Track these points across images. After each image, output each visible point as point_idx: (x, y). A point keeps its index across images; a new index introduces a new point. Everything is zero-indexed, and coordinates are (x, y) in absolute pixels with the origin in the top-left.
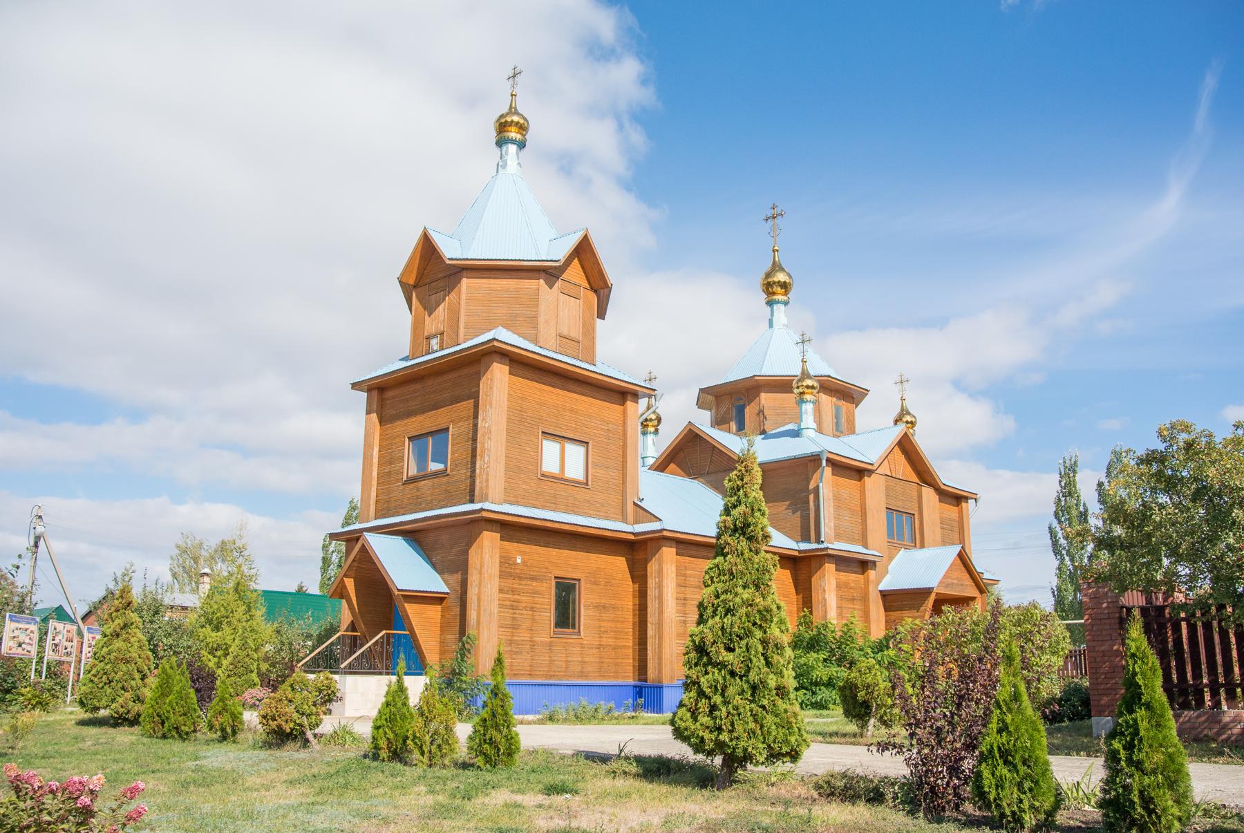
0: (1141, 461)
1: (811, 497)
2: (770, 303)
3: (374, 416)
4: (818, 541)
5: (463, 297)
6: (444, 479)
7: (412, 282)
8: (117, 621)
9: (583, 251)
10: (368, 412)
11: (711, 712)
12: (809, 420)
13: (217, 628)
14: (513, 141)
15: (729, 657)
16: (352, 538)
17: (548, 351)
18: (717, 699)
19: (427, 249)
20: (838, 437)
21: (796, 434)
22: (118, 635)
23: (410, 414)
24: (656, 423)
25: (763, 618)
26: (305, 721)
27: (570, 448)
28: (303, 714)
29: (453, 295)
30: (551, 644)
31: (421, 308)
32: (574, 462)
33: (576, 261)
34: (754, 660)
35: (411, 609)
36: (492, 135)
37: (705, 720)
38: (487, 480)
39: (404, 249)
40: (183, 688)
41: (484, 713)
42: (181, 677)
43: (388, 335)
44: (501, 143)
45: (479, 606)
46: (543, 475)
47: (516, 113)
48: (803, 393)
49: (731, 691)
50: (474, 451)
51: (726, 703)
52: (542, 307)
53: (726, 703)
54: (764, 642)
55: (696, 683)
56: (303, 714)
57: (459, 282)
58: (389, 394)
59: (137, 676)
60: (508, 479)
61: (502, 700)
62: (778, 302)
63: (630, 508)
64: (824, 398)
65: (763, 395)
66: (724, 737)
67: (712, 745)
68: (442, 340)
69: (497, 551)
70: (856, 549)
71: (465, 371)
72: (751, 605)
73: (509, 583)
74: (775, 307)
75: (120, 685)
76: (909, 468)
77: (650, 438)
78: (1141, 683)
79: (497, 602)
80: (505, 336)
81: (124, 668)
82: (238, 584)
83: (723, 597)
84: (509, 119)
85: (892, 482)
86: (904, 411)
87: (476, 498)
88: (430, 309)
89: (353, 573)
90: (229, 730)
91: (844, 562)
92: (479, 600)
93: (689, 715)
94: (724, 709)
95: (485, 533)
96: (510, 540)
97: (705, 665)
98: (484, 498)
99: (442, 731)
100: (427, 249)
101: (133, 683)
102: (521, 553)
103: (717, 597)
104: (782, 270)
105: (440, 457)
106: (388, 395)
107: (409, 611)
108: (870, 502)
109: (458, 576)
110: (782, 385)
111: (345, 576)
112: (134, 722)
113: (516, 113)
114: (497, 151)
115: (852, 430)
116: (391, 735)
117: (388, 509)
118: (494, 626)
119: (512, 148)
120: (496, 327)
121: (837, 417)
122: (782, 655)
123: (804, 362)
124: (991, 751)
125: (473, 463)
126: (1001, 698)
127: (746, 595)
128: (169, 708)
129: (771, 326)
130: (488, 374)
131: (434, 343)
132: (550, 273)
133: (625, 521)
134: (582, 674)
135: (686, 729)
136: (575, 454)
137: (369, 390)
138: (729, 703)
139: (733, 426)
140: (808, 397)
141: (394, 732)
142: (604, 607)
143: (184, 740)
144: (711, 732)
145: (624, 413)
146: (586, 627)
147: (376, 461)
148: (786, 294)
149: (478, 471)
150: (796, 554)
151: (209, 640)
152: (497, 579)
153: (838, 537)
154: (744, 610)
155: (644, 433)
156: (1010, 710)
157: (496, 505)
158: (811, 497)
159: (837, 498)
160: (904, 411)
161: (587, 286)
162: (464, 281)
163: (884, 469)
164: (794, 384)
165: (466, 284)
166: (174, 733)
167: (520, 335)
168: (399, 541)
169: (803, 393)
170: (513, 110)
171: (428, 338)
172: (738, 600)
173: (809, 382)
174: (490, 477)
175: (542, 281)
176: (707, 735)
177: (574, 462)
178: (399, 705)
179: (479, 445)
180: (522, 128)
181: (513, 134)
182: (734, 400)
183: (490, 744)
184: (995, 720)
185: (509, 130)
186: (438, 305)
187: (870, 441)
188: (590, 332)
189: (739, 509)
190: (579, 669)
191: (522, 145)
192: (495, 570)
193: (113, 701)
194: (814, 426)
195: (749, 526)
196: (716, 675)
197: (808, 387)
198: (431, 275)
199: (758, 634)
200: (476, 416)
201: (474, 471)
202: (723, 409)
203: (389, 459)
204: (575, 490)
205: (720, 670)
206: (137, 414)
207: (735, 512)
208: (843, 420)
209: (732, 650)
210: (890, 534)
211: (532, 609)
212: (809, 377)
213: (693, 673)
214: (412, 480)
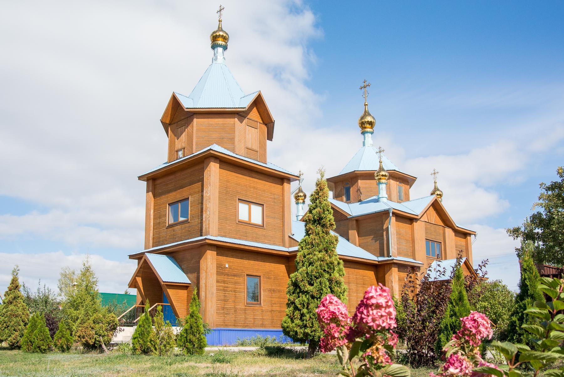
0: (548, 189)
1: (385, 233)
2: (363, 133)
3: (150, 193)
4: (389, 256)
5: (195, 129)
6: (187, 225)
7: (168, 122)
8: (11, 296)
9: (258, 103)
10: (148, 192)
11: (301, 318)
12: (383, 193)
13: (77, 309)
14: (220, 46)
15: (310, 288)
16: (139, 257)
17: (239, 154)
18: (305, 311)
19: (175, 103)
20: (400, 203)
21: (377, 201)
22: (11, 303)
23: (169, 192)
24: (303, 198)
25: (329, 267)
26: (101, 339)
27: (253, 207)
28: (100, 335)
29: (189, 128)
30: (245, 310)
31: (173, 136)
32: (256, 215)
33: (255, 108)
34: (324, 289)
35: (171, 292)
36: (209, 43)
37: (297, 321)
38: (209, 224)
39: (164, 103)
40: (42, 327)
41: (187, 326)
42: (46, 327)
43: (157, 152)
44: (214, 47)
45: (206, 289)
46: (239, 222)
47: (222, 30)
48: (380, 179)
49: (312, 306)
50: (202, 209)
51: (309, 312)
52: (237, 133)
53: (309, 312)
54: (330, 281)
55: (293, 303)
56: (100, 335)
57: (192, 121)
58: (158, 182)
59: (22, 324)
60: (220, 223)
61: (196, 320)
62: (367, 132)
63: (287, 238)
64: (392, 182)
65: (359, 181)
66: (308, 330)
67: (301, 336)
68: (184, 152)
69: (215, 261)
70: (409, 260)
71: (197, 167)
72: (323, 261)
73: (221, 278)
74: (366, 135)
75: (13, 328)
76: (438, 219)
77: (300, 206)
78: (528, 284)
79: (215, 288)
80: (217, 148)
81: (15, 320)
82: (87, 286)
83: (307, 257)
84: (218, 34)
85: (429, 226)
86: (436, 189)
87: (203, 234)
88: (178, 136)
89: (141, 275)
90: (65, 347)
91: (402, 266)
92: (206, 286)
93: (289, 320)
94: (308, 316)
95: (208, 251)
96: (222, 255)
97: (298, 293)
98: (209, 234)
99: (166, 337)
100: (175, 103)
101: (20, 327)
102: (228, 262)
103: (305, 257)
104: (369, 115)
105: (184, 214)
106: (156, 181)
107: (170, 293)
108: (416, 236)
109: (195, 275)
110: (369, 176)
111: (137, 276)
112: (19, 348)
113: (222, 30)
114: (212, 51)
115: (407, 199)
116: (141, 342)
117: (159, 242)
118: (214, 300)
119: (220, 50)
120: (212, 144)
121: (399, 192)
122: (340, 287)
123: (380, 162)
124: (446, 327)
125: (202, 215)
126: (452, 298)
127: (320, 255)
128: (34, 337)
129: (364, 145)
130: (208, 169)
131: (180, 154)
132: (240, 114)
133: (284, 246)
134: (263, 325)
135: (288, 327)
136: (257, 211)
137: (148, 180)
138: (311, 312)
139: (344, 198)
140: (383, 181)
141: (143, 341)
142: (274, 291)
143: (43, 353)
144: (301, 328)
145: (283, 189)
146: (264, 301)
147: (152, 217)
148: (372, 128)
149: (204, 219)
150: (377, 263)
151: (73, 315)
152: (215, 276)
153: (399, 254)
154: (319, 263)
155: (297, 203)
156: (457, 304)
157: (213, 235)
158: (385, 233)
159: (398, 233)
160: (436, 189)
161: (261, 122)
162: (195, 120)
163: (425, 218)
164: (375, 175)
165: (196, 121)
166: (38, 350)
167: (225, 148)
168: (164, 258)
169: (380, 179)
170: (220, 29)
171: (177, 151)
172: (315, 258)
173: (383, 173)
174: (211, 223)
175: (236, 119)
176: (298, 330)
177: (256, 215)
178: (146, 326)
179: (204, 206)
180: (225, 39)
181: (220, 42)
182: (345, 184)
183: (190, 342)
184: (449, 310)
185: (218, 40)
186: (182, 134)
187: (417, 203)
188: (263, 147)
189: (316, 210)
190: (261, 323)
191: (225, 48)
192: (214, 271)
193: (10, 336)
194: (386, 196)
195: (322, 219)
196: (304, 298)
197: (383, 175)
198: (177, 117)
199: (327, 276)
200: (202, 191)
201: (202, 220)
202: (339, 189)
203: (159, 216)
204: (257, 230)
205: (306, 296)
206: (45, 210)
207: (314, 212)
208: (403, 194)
209: (312, 285)
210: (428, 253)
211: (235, 291)
212: (383, 170)
213: (292, 298)
214: (171, 226)
